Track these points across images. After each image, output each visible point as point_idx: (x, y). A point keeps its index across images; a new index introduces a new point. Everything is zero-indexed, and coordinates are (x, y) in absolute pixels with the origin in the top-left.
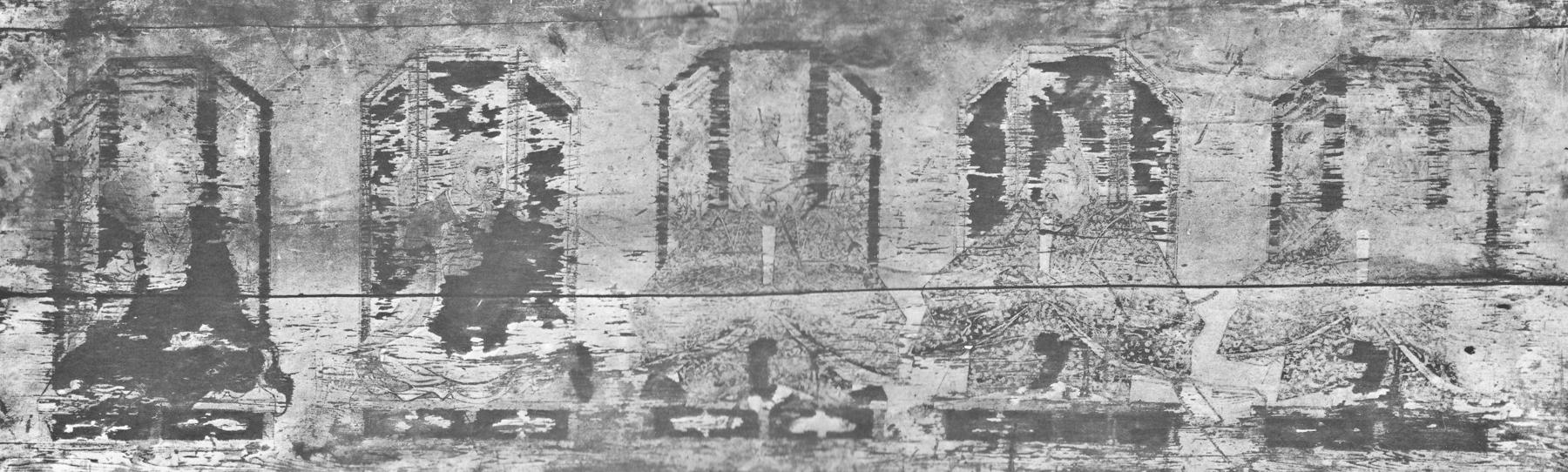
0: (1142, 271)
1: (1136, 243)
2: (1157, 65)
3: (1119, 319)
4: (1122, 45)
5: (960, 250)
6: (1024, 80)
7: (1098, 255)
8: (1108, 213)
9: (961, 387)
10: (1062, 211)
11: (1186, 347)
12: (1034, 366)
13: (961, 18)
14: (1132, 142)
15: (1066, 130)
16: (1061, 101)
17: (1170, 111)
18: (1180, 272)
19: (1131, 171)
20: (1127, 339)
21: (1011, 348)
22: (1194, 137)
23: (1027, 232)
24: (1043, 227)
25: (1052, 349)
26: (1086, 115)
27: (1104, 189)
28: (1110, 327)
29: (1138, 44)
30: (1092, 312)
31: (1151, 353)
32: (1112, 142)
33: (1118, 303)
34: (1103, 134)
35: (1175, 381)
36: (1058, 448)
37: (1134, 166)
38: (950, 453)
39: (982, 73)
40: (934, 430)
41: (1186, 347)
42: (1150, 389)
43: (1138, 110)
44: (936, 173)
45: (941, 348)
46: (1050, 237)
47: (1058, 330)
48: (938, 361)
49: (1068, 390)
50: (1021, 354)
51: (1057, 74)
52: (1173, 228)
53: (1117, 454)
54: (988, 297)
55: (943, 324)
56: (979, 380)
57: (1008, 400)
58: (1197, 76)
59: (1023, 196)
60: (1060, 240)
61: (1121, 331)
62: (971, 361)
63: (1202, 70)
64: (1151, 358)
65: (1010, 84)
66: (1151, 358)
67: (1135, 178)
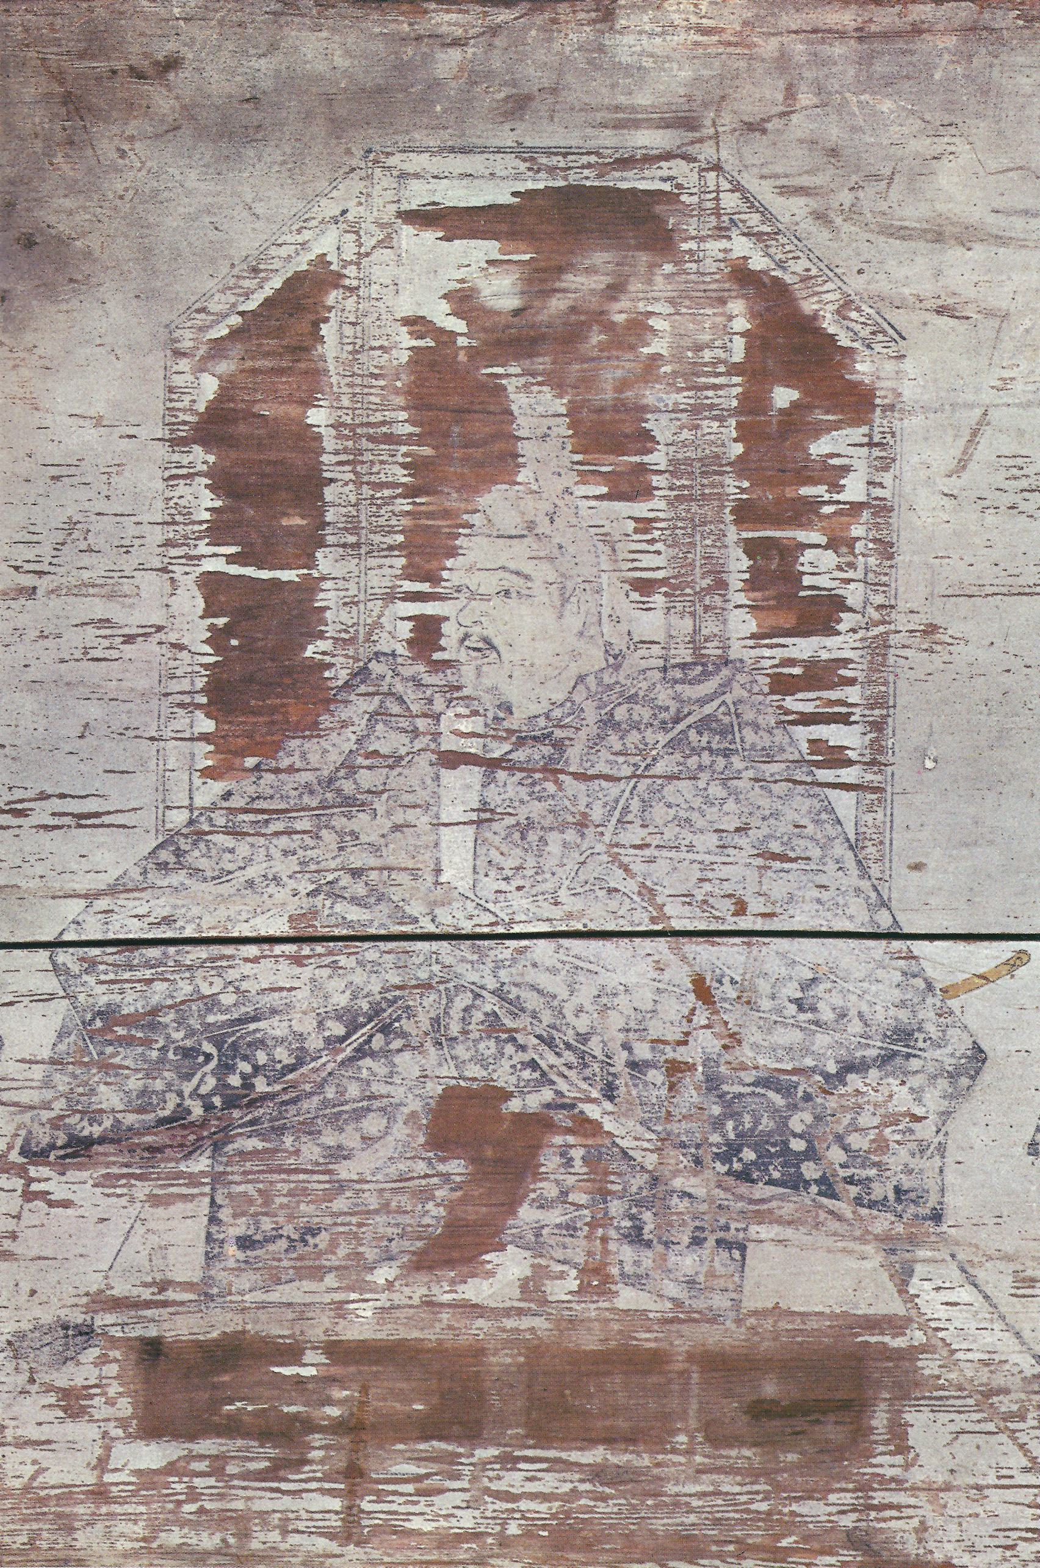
0: (778, 888)
1: (757, 796)
2: (821, 217)
3: (706, 1043)
4: (707, 152)
5: (178, 818)
6: (381, 268)
7: (634, 834)
8: (663, 696)
9: (186, 1265)
10: (513, 693)
11: (925, 1131)
12: (425, 1195)
13: (172, 64)
14: (741, 466)
15: (523, 425)
16: (515, 339)
17: (863, 369)
18: (905, 887)
19: (738, 564)
20: (731, 1107)
21: (350, 1138)
22: (943, 454)
23: (396, 761)
24: (449, 743)
25: (487, 1142)
26: (587, 382)
27: (652, 621)
28: (675, 1068)
29: (758, 149)
30: (616, 1021)
31: (811, 1154)
32: (675, 468)
33: (702, 990)
34: (645, 440)
35: (889, 1244)
36: (509, 1462)
37: (751, 548)
38: (148, 1479)
39: (246, 241)
40: (99, 1407)
41: (925, 1131)
42: (808, 1275)
43: (756, 373)
44: (97, 568)
45: (116, 1137)
46: (473, 775)
47: (504, 1077)
48: (108, 1181)
49: (540, 1273)
50: (384, 1157)
51: (491, 248)
52: (877, 746)
53: (699, 1483)
54: (266, 973)
55: (125, 1057)
56: (245, 1243)
57: (339, 1309)
58: (955, 254)
59: (385, 645)
60: (508, 788)
61: (712, 1083)
62: (218, 1179)
63: (967, 236)
64: (810, 1171)
65: (335, 280)
66: (810, 1171)
67: (752, 584)
